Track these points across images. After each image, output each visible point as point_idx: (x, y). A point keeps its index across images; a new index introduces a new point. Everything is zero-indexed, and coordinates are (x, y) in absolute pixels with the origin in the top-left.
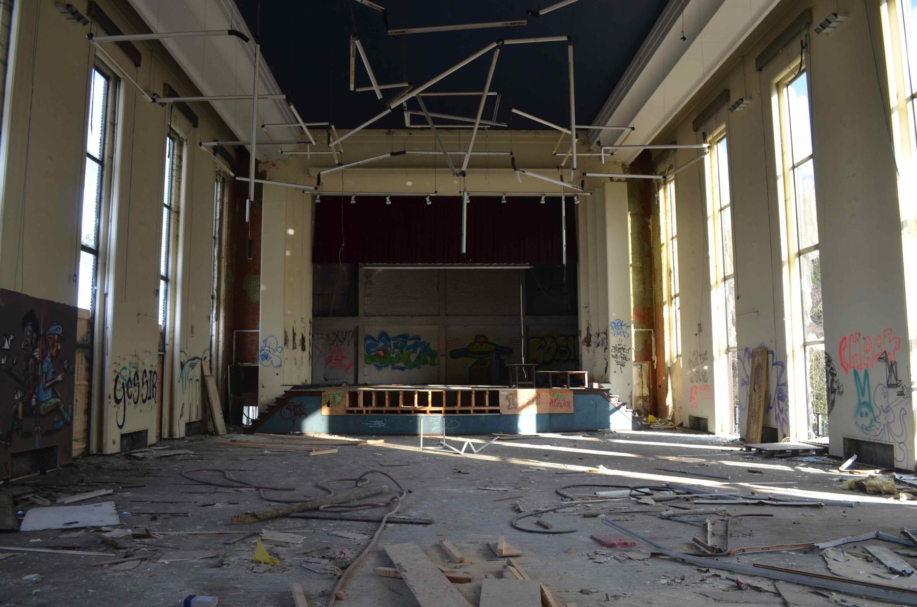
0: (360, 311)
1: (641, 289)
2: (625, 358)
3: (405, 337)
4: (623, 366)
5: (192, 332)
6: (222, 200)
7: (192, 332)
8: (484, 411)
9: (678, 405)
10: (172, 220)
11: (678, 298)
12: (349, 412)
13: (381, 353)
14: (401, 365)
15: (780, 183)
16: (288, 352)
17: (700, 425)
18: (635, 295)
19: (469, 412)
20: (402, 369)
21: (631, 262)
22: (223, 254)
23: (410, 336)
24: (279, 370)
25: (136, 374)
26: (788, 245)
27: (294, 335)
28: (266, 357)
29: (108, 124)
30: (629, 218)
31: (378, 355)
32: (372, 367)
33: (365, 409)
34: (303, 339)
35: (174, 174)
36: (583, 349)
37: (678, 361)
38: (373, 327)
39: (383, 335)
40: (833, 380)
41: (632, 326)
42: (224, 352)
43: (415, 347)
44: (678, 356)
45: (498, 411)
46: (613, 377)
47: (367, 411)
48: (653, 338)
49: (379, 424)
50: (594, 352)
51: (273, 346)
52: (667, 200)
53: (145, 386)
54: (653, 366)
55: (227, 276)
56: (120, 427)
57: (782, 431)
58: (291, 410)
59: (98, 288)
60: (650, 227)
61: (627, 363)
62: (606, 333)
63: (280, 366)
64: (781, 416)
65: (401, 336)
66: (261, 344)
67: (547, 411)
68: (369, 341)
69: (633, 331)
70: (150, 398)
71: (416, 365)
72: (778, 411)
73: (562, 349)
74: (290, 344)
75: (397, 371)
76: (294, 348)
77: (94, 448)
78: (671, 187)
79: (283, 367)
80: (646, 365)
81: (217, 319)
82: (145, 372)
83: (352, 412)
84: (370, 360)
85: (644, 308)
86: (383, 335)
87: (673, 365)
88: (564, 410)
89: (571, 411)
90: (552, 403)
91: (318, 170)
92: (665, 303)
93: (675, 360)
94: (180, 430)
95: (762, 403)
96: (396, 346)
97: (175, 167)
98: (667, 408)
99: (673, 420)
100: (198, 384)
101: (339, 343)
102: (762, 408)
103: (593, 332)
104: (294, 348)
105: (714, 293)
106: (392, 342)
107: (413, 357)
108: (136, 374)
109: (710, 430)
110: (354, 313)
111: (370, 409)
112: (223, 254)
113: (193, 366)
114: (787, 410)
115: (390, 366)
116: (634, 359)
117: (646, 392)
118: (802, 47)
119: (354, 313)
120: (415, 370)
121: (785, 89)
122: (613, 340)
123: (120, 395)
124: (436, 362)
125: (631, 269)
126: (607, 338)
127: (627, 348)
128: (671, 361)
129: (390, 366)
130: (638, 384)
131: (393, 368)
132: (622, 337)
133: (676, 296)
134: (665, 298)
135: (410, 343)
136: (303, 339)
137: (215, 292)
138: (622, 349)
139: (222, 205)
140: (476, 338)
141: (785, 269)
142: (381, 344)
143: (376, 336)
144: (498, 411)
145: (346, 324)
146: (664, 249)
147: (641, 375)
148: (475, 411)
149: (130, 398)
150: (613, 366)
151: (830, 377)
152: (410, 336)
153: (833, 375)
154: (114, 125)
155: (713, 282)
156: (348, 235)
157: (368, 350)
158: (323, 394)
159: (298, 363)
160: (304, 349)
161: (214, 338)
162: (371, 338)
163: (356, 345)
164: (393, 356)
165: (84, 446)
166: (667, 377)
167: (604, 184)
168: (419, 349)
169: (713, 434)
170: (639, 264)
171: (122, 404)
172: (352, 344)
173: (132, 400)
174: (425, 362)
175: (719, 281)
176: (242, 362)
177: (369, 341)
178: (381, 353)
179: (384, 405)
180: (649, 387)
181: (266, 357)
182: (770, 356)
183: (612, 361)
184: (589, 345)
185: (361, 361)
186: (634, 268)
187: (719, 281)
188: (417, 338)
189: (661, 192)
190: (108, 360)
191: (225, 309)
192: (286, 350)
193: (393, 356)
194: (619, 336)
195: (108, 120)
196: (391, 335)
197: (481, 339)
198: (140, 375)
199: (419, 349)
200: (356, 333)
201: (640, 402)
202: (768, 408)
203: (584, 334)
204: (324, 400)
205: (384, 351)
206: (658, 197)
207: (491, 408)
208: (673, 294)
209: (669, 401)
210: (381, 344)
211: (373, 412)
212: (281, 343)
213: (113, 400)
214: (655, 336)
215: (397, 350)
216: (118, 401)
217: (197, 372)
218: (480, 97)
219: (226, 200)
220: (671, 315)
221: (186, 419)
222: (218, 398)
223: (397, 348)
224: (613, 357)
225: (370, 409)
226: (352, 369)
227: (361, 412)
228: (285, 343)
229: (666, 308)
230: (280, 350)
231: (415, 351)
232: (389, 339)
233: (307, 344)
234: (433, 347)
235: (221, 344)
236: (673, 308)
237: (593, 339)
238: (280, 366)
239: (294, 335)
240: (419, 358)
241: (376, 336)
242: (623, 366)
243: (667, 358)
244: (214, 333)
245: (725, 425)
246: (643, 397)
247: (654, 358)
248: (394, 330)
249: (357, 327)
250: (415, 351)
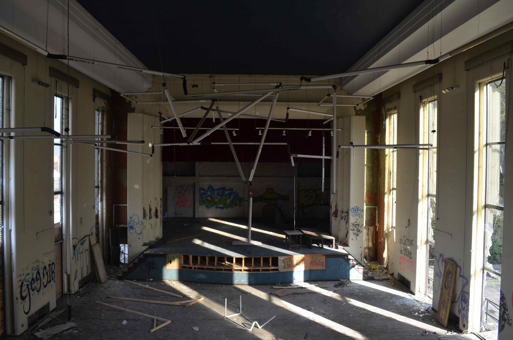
2: (359, 231)
3: (223, 189)
4: (358, 235)
5: (81, 222)
6: (102, 123)
7: (81, 222)
8: (268, 270)
10: (64, 153)
12: (183, 267)
13: (209, 198)
14: (221, 206)
15: (476, 156)
16: (147, 222)
17: (405, 285)
18: (367, 184)
19: (259, 270)
20: (222, 208)
21: (366, 163)
22: (104, 158)
25: (38, 273)
26: (478, 199)
27: (150, 210)
28: (132, 228)
29: (5, 111)
30: (366, 135)
32: (204, 207)
33: (193, 267)
34: (156, 211)
35: (64, 121)
36: (333, 218)
37: (393, 231)
39: (211, 187)
40: (504, 312)
42: (106, 222)
44: (392, 227)
46: (351, 243)
47: (195, 268)
48: (377, 212)
49: (202, 276)
50: (339, 222)
52: (391, 126)
53: (46, 276)
54: (376, 229)
55: (107, 173)
56: (26, 313)
57: (463, 321)
59: (5, 226)
61: (360, 234)
62: (348, 213)
63: (141, 233)
64: (463, 312)
65: (220, 188)
66: (128, 219)
67: (309, 269)
68: (202, 191)
69: (365, 207)
70: (50, 281)
72: (460, 307)
74: (148, 217)
75: (219, 209)
76: (150, 218)
77: (9, 331)
78: (394, 118)
80: (371, 228)
81: (102, 200)
82: (45, 267)
83: (186, 267)
84: (202, 202)
86: (211, 187)
87: (389, 232)
88: (319, 268)
89: (324, 268)
90: (312, 263)
92: (386, 193)
93: (390, 230)
94: (75, 287)
95: (450, 298)
96: (218, 194)
97: (64, 117)
98: (383, 259)
99: (387, 268)
100: (87, 253)
102: (450, 302)
103: (340, 209)
104: (150, 218)
105: (420, 205)
107: (228, 201)
108: (38, 273)
109: (412, 289)
111: (197, 266)
112: (104, 158)
113: (82, 244)
114: (468, 310)
116: (364, 225)
117: (371, 245)
118: (505, 68)
119: (194, 175)
121: (485, 87)
122: (352, 219)
123: (24, 294)
125: (366, 167)
126: (348, 215)
127: (360, 225)
128: (388, 229)
130: (366, 240)
132: (358, 218)
133: (393, 189)
135: (227, 192)
136: (156, 211)
137: (99, 184)
138: (357, 225)
139: (102, 126)
141: (475, 217)
142: (209, 193)
143: (206, 188)
144: (277, 270)
145: (187, 181)
146: (387, 158)
147: (368, 234)
148: (263, 270)
149: (33, 290)
151: (503, 309)
153: (506, 309)
154: (9, 110)
155: (420, 197)
158: (167, 256)
159: (153, 227)
160: (157, 217)
161: (100, 213)
162: (203, 189)
164: (217, 200)
165: (2, 331)
166: (384, 239)
168: (232, 197)
169: (414, 294)
171: (27, 299)
173: (35, 291)
175: (424, 196)
176: (119, 224)
177: (202, 191)
178: (209, 198)
179: (205, 265)
180: (373, 242)
181: (132, 228)
182: (458, 269)
183: (351, 233)
184: (336, 216)
185: (197, 203)
186: (368, 167)
187: (424, 196)
188: (231, 190)
190: (14, 275)
192: (144, 221)
193: (217, 200)
195: (5, 107)
196: (215, 188)
198: (41, 272)
199: (232, 197)
200: (194, 186)
201: (367, 251)
202: (453, 302)
203: (333, 209)
204: (167, 259)
206: (385, 124)
207: (273, 268)
208: (391, 188)
209: (385, 255)
210: (209, 193)
211: (198, 268)
212: (141, 215)
213: (20, 300)
214: (379, 211)
215: (218, 197)
216: (23, 298)
217: (86, 245)
221: (79, 278)
222: (101, 258)
225: (197, 266)
226: (192, 208)
227: (191, 268)
229: (386, 196)
231: (230, 198)
232: (214, 190)
234: (241, 195)
235: (104, 216)
237: (339, 213)
238: (141, 233)
239: (150, 210)
241: (206, 188)
242: (358, 235)
245: (423, 292)
246: (369, 248)
247: (377, 224)
248: (217, 185)
250: (230, 198)
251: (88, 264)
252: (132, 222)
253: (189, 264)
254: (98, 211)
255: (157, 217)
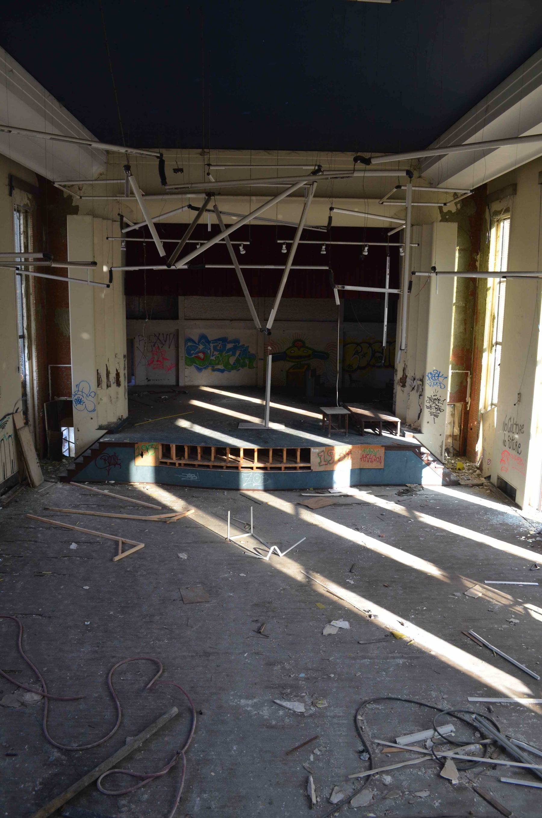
0: (181, 314)
1: (462, 330)
2: (439, 409)
3: (224, 340)
4: (437, 416)
8: (295, 468)
9: (487, 458)
11: (499, 348)
12: (162, 463)
13: (201, 355)
14: (220, 367)
16: (104, 393)
18: (455, 335)
19: (280, 469)
20: (222, 371)
21: (454, 301)
23: (230, 339)
24: (93, 415)
27: (108, 373)
28: (79, 401)
31: (199, 358)
34: (118, 375)
36: (398, 389)
37: (492, 410)
38: (195, 331)
41: (450, 366)
42: (39, 391)
43: (234, 349)
44: (492, 404)
45: (309, 468)
46: (425, 428)
47: (180, 464)
48: (469, 380)
49: (192, 477)
51: (86, 391)
54: (466, 407)
58: (105, 460)
60: (478, 264)
61: (441, 415)
62: (422, 380)
63: (94, 410)
65: (219, 339)
66: (74, 389)
68: (189, 344)
69: (450, 372)
71: (235, 367)
73: (378, 355)
74: (104, 385)
75: (216, 373)
76: (108, 386)
78: (506, 225)
79: (98, 405)
80: (459, 405)
81: (30, 358)
84: (191, 362)
85: (463, 350)
86: (203, 338)
87: (487, 412)
88: (375, 465)
89: (382, 466)
90: (363, 458)
91: (123, 199)
93: (489, 408)
96: (215, 349)
98: (475, 453)
99: (480, 468)
100: (11, 441)
101: (160, 346)
103: (410, 374)
104: (108, 386)
106: (212, 345)
107: (232, 360)
109: (518, 500)
110: (176, 317)
111: (183, 462)
115: (210, 368)
116: (448, 400)
117: (456, 431)
119: (176, 317)
120: (234, 372)
122: (429, 391)
124: (254, 365)
125: (454, 307)
127: (442, 399)
129: (210, 368)
130: (450, 423)
131: (214, 370)
132: (438, 388)
133: (497, 343)
134: (486, 345)
135: (229, 346)
136: (118, 375)
137: (25, 331)
139: (26, 237)
140: (295, 342)
142: (201, 347)
143: (196, 339)
144: (309, 468)
145: (166, 326)
146: (489, 293)
147: (453, 415)
150: (427, 415)
152: (230, 339)
156: (155, 286)
157: (188, 352)
158: (136, 446)
160: (118, 384)
161: (28, 378)
163: (177, 347)
164: (213, 358)
166: (479, 423)
167: (432, 223)
168: (238, 353)
170: (462, 304)
172: (173, 347)
174: (243, 366)
177: (189, 344)
178: (201, 355)
180: (460, 427)
181: (79, 401)
183: (426, 412)
184: (404, 386)
185: (182, 363)
186: (457, 307)
188: (236, 341)
189: (493, 230)
191: (38, 350)
193: (213, 358)
194: (435, 387)
196: (210, 338)
197: (298, 343)
199: (238, 353)
200: (176, 335)
201: (450, 440)
203: (399, 375)
205: (204, 353)
206: (489, 237)
208: (494, 341)
209: (479, 447)
210: (201, 347)
211: (186, 465)
214: (472, 378)
218: (282, 271)
219: (30, 232)
220: (491, 362)
223: (217, 351)
224: (428, 408)
225: (183, 462)
226: (174, 370)
227: (174, 464)
228: (99, 384)
229: (485, 355)
230: (93, 394)
231: (234, 354)
232: (209, 342)
233: (122, 379)
234: (252, 351)
236: (492, 356)
237: (409, 381)
238: (94, 410)
239: (108, 373)
240: (238, 360)
241: (196, 339)
242: (437, 416)
243: (481, 406)
244: (27, 372)
246: (453, 437)
247: (468, 399)
248: (213, 333)
249: (178, 330)
250: (234, 354)
251: (12, 458)
252: (80, 393)
253: (169, 457)
254: (25, 376)
255: (118, 384)
